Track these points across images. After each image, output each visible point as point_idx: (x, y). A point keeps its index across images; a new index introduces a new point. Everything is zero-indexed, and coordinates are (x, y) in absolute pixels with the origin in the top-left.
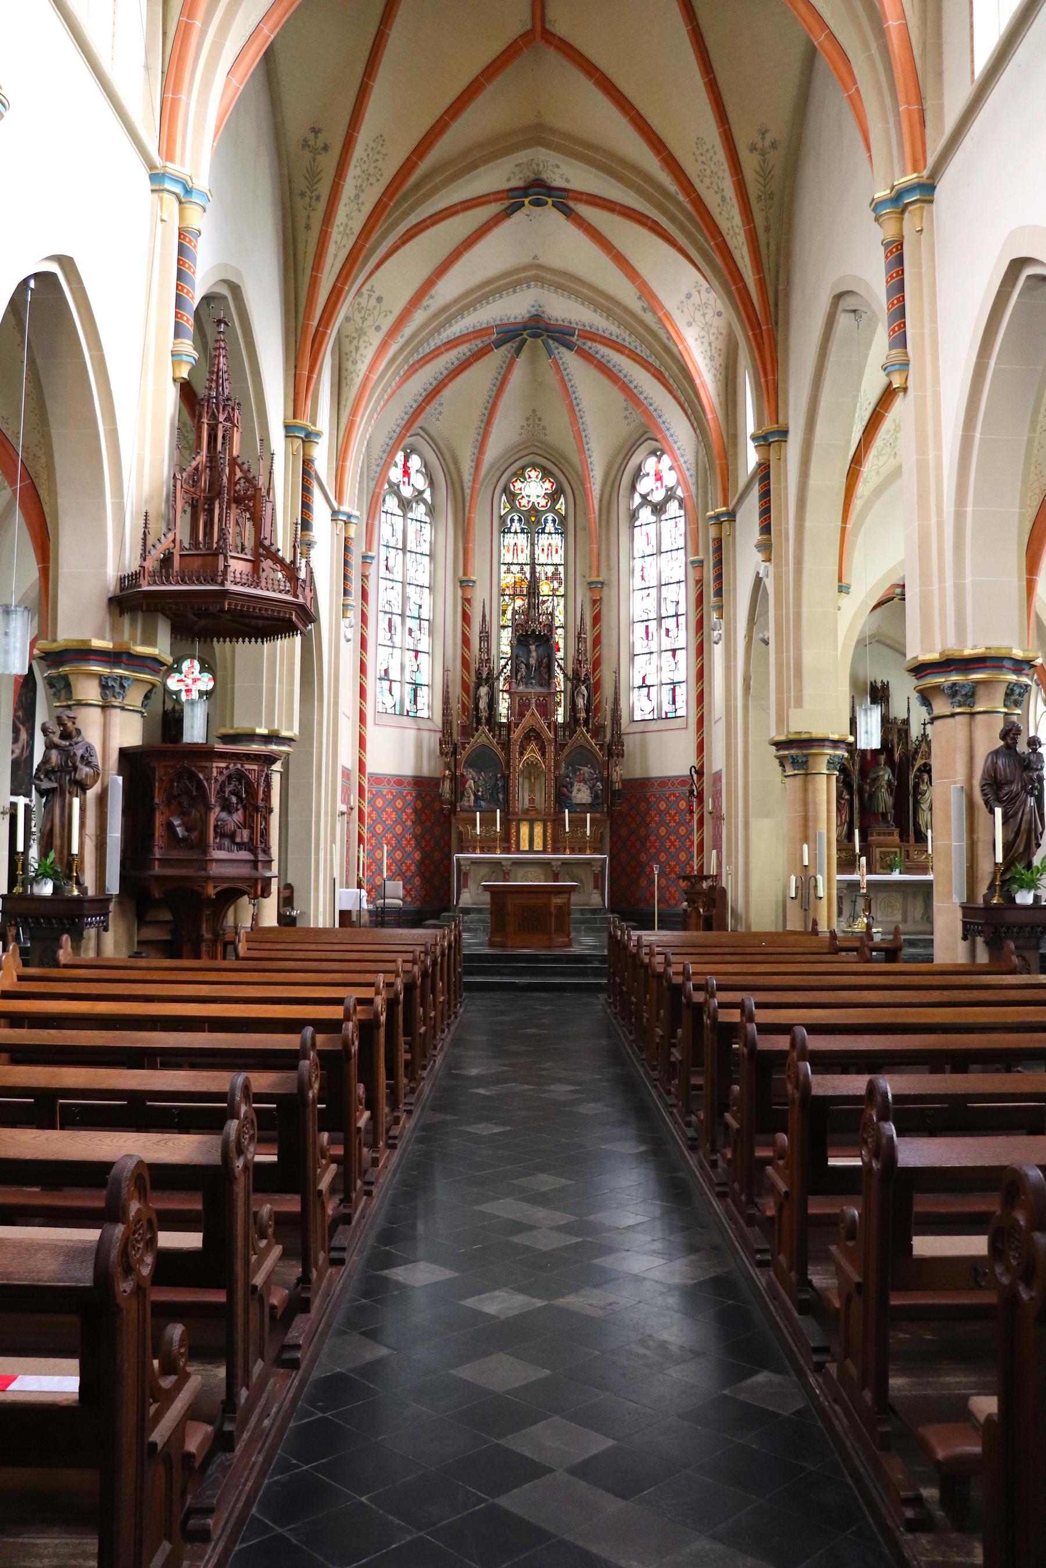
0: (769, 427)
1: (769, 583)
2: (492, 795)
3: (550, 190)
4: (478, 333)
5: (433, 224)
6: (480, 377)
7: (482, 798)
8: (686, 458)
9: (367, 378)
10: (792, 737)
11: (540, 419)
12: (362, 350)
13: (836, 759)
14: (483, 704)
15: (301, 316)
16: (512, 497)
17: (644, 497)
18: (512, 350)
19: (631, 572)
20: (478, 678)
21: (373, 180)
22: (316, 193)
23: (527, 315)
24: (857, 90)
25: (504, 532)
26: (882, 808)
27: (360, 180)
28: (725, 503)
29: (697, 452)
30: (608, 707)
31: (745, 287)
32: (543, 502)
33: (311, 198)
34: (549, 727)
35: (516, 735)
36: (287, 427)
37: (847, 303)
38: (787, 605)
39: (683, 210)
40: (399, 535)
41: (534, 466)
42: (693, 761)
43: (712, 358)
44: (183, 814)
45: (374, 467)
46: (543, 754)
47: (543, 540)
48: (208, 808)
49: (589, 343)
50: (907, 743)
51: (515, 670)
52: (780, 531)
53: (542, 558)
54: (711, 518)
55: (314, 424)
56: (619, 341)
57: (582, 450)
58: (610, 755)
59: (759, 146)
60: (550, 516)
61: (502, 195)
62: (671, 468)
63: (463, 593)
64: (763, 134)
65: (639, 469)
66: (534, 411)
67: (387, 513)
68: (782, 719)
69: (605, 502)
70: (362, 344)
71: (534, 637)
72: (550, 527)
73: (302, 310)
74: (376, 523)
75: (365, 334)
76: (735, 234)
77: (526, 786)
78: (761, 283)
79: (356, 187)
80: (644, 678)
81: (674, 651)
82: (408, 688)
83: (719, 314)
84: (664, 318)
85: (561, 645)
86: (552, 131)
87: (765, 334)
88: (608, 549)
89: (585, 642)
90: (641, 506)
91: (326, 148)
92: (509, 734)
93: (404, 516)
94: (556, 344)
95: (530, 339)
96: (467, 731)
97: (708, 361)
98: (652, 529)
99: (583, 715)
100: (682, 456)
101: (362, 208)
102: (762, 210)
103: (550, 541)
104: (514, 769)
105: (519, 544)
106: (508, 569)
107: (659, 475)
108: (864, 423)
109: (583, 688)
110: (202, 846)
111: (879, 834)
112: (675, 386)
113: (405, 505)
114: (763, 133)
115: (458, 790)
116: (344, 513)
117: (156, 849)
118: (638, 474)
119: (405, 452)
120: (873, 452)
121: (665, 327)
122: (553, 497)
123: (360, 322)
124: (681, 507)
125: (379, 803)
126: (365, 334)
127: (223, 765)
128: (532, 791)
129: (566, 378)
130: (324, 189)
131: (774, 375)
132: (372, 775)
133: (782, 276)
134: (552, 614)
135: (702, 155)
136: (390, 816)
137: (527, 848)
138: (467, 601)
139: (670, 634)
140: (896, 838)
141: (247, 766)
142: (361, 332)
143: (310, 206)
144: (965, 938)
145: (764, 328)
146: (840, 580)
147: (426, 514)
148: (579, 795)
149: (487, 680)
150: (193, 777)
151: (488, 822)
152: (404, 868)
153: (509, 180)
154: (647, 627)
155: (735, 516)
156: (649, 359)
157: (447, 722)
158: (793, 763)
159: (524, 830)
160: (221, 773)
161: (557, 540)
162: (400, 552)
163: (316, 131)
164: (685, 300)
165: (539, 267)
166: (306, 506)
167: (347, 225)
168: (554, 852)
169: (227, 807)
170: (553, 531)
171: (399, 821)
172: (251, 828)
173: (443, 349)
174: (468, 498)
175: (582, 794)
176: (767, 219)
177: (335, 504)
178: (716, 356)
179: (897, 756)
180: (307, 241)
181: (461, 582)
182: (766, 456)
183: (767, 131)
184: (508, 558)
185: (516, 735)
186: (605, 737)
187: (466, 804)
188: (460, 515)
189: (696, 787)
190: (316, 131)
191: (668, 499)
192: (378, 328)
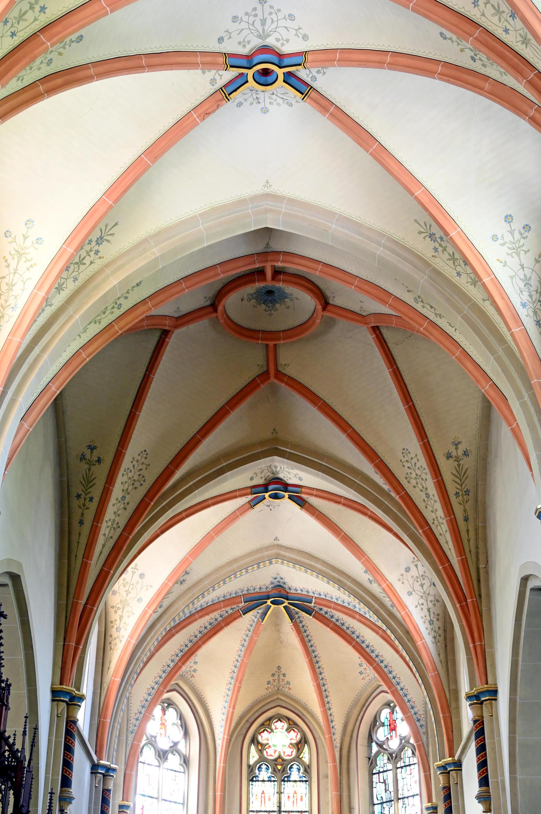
0: (480, 687)
3: (285, 486)
4: (228, 601)
5: (188, 516)
11: (284, 675)
12: (125, 619)
15: (71, 596)
16: (261, 747)
18: (258, 615)
21: (137, 484)
22: (90, 495)
24: (517, 424)
27: (126, 485)
31: (451, 566)
32: (288, 751)
33: (85, 499)
39: (396, 503)
43: (431, 622)
45: (134, 721)
49: (325, 609)
52: (497, 782)
55: (78, 689)
56: (350, 607)
59: (454, 454)
61: (245, 491)
64: (456, 445)
67: (144, 763)
70: (125, 614)
73: (72, 591)
75: (128, 605)
76: (440, 524)
78: (464, 563)
79: (123, 490)
86: (285, 443)
91: (99, 461)
95: (273, 606)
97: (427, 625)
98: (390, 776)
100: (412, 708)
101: (128, 507)
102: (460, 504)
103: (295, 789)
113: (162, 755)
114: (456, 445)
116: (104, 766)
122: (299, 746)
123: (124, 594)
126: (128, 605)
129: (306, 639)
130: (96, 493)
131: (481, 641)
135: (407, 461)
143: (84, 505)
145: (469, 600)
153: (252, 479)
155: (461, 765)
156: (377, 623)
163: (92, 448)
164: (405, 573)
165: (280, 546)
166: (67, 764)
167: (114, 520)
173: (197, 616)
176: (465, 511)
177: (95, 758)
178: (435, 620)
180: (80, 534)
182: (479, 714)
183: (459, 443)
190: (92, 448)
191: (402, 749)
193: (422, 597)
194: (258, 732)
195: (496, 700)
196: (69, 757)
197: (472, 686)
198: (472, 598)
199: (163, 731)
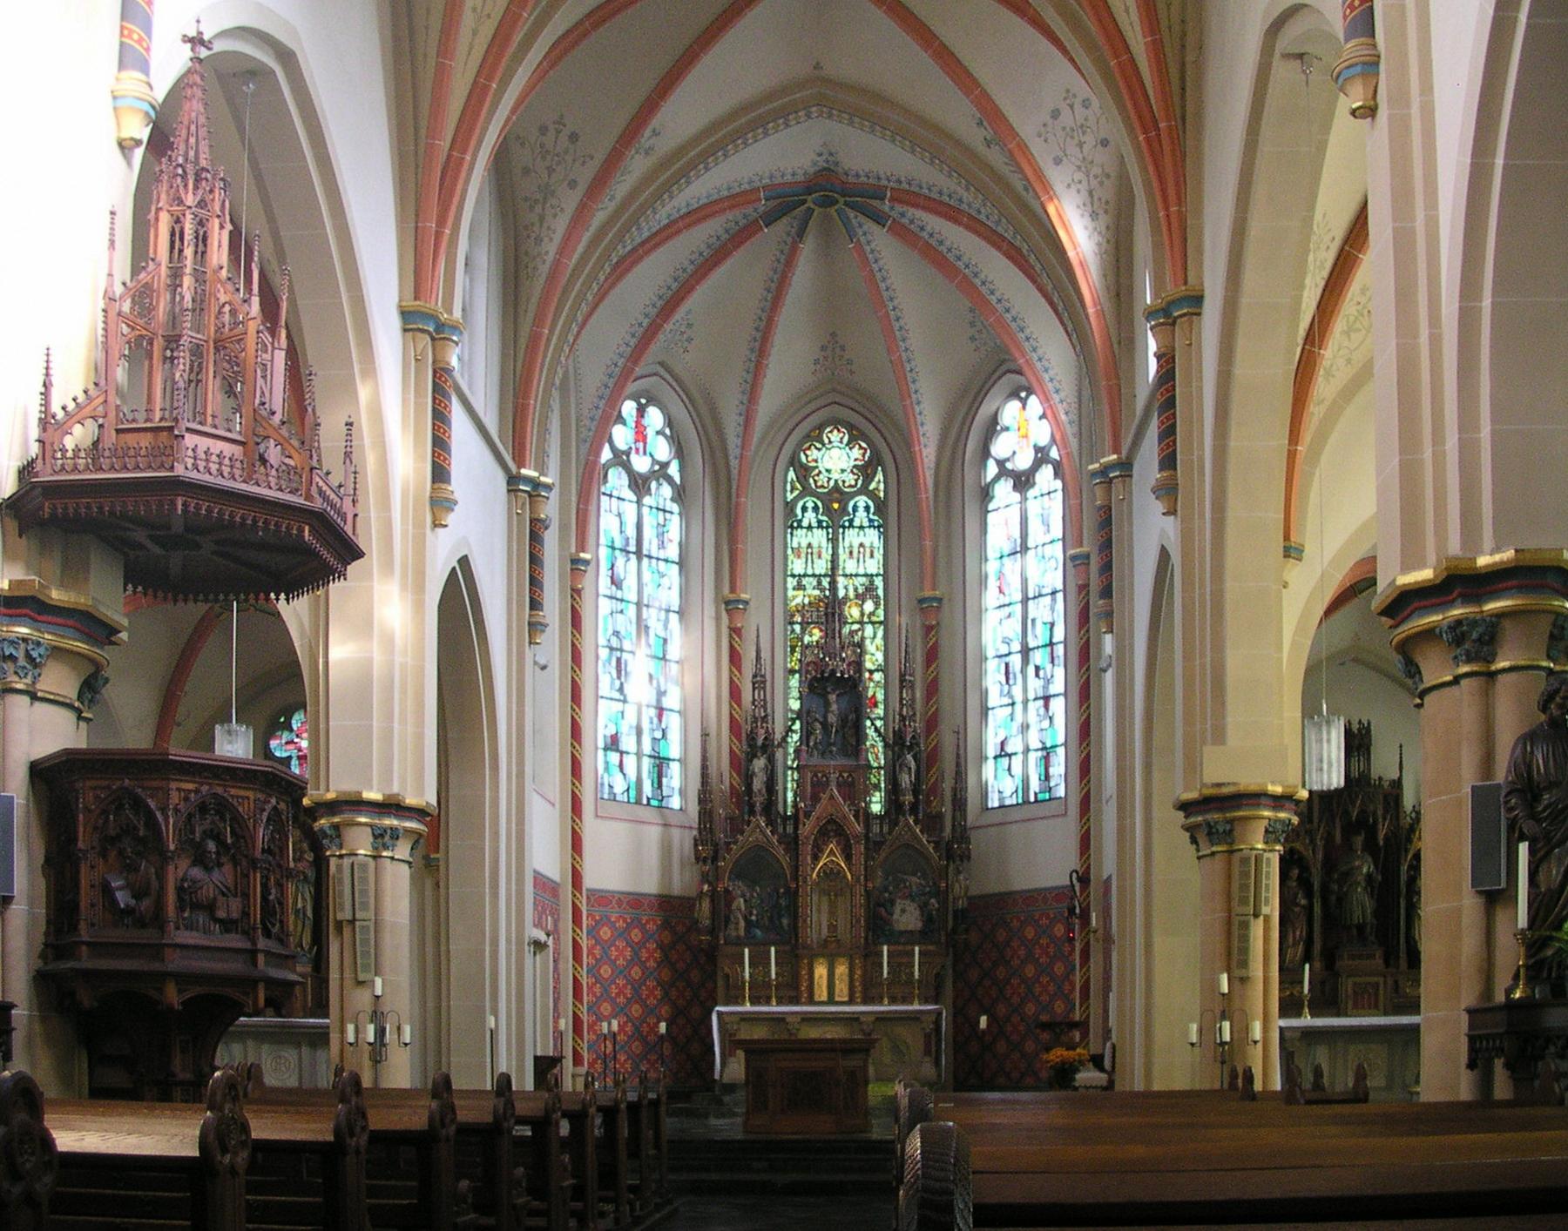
0: (1172, 290)
1: (1176, 559)
2: (771, 919)
4: (736, 199)
6: (742, 275)
7: (757, 925)
8: (1063, 394)
9: (557, 264)
10: (1208, 792)
11: (843, 348)
13: (1279, 826)
14: (758, 783)
15: (423, 132)
16: (804, 472)
17: (1001, 463)
19: (983, 581)
20: (750, 746)
23: (812, 170)
25: (792, 527)
26: (1357, 917)
28: (1116, 450)
29: (1080, 392)
30: (947, 785)
31: (1132, 60)
34: (856, 816)
35: (807, 828)
36: (406, 315)
37: (1288, 39)
38: (1202, 580)
40: (631, 532)
41: (836, 423)
42: (1072, 861)
44: (129, 868)
45: (587, 422)
46: (848, 858)
47: (852, 537)
48: (164, 857)
50: (1398, 818)
51: (806, 734)
53: (850, 566)
54: (1094, 474)
57: (905, 394)
58: (950, 856)
60: (862, 501)
62: (1043, 416)
63: (731, 621)
65: (994, 420)
66: (833, 335)
67: (611, 496)
68: (1193, 765)
69: (943, 473)
71: (835, 683)
72: (861, 517)
73: (423, 123)
74: (592, 508)
77: (825, 907)
78: (1157, 50)
80: (1002, 744)
81: (1047, 699)
82: (647, 763)
83: (1105, 143)
84: (1017, 151)
85: (880, 696)
87: (1164, 135)
88: (949, 547)
89: (912, 687)
90: (997, 478)
92: (796, 828)
93: (639, 503)
94: (862, 218)
95: (818, 210)
96: (736, 826)
99: (909, 798)
100: (1057, 391)
103: (862, 539)
104: (805, 882)
105: (815, 545)
106: (799, 583)
107: (1023, 429)
108: (1325, 273)
109: (909, 757)
110: (157, 919)
111: (1352, 957)
112: (1038, 267)
113: (640, 485)
115: (721, 915)
117: (82, 926)
118: (992, 428)
119: (639, 404)
120: (1339, 326)
121: (1022, 171)
122: (865, 471)
124: (1056, 475)
125: (606, 933)
126: (553, 193)
127: (191, 786)
128: (832, 913)
132: (591, 892)
133: (1191, 40)
134: (861, 645)
136: (621, 954)
137: (824, 997)
138: (735, 631)
139: (1041, 673)
140: (1379, 961)
141: (233, 791)
142: (547, 192)
144: (1471, 1065)
145: (1162, 125)
146: (1287, 537)
147: (672, 500)
148: (904, 919)
149: (764, 748)
150: (138, 805)
151: (759, 961)
152: (645, 1029)
154: (1007, 665)
155: (1131, 465)
157: (706, 814)
158: (1210, 834)
159: (821, 971)
160: (186, 799)
161: (872, 537)
162: (633, 557)
164: (1050, 121)
165: (827, 81)
166: (440, 444)
168: (865, 1002)
169: (200, 860)
170: (866, 523)
171: (636, 960)
172: (246, 896)
174: (735, 472)
175: (907, 917)
179: (1381, 836)
181: (727, 603)
184: (797, 566)
185: (807, 828)
186: (942, 830)
187: (734, 934)
188: (723, 496)
189: (1078, 908)
192: (573, 184)
193: (1079, 168)
194: (799, 448)
195: (1199, 314)
196: (136, 37)
197: (1155, 295)
198: (1169, 120)
199: (641, 445)
